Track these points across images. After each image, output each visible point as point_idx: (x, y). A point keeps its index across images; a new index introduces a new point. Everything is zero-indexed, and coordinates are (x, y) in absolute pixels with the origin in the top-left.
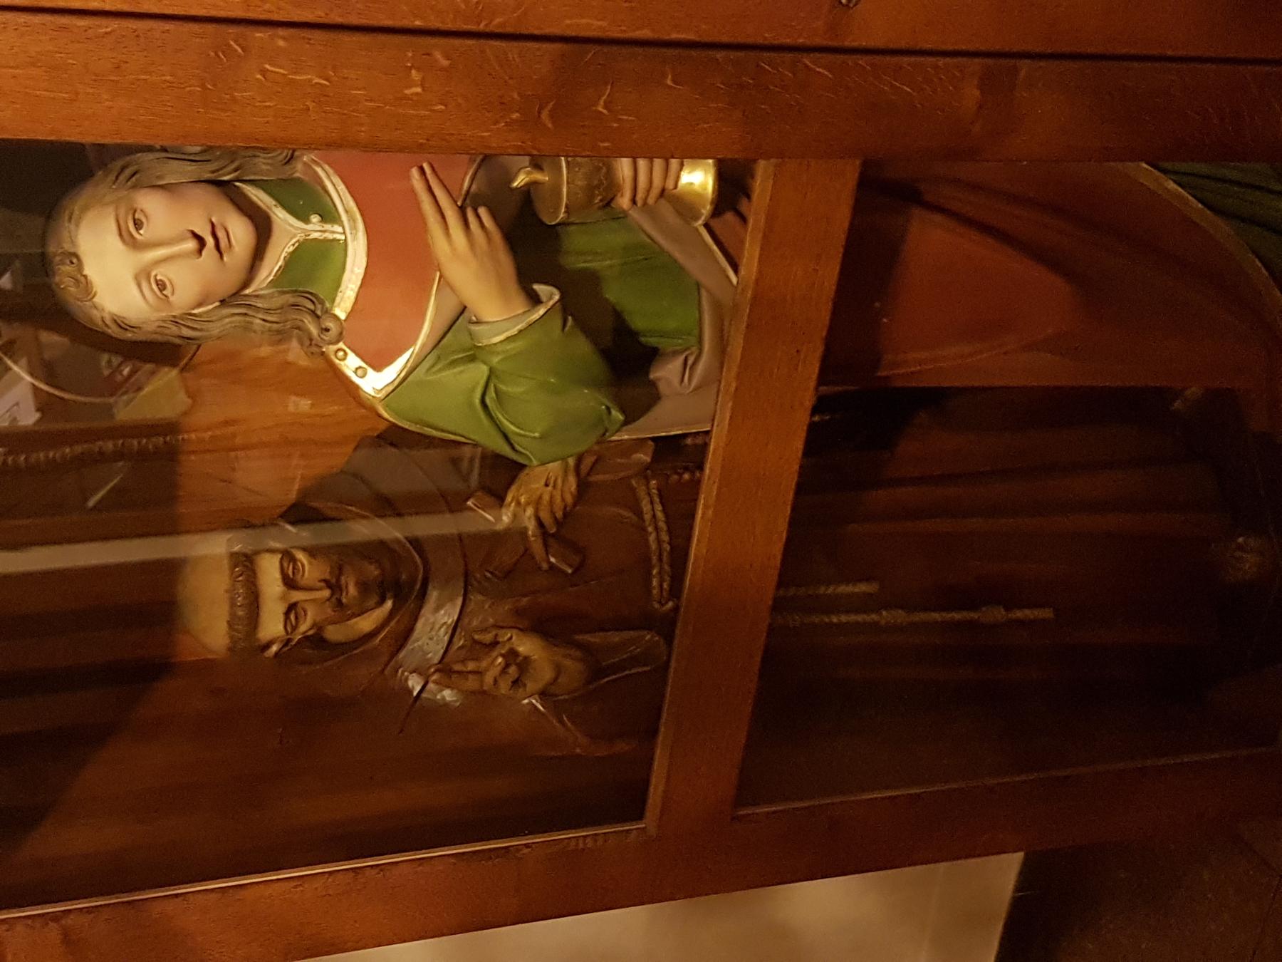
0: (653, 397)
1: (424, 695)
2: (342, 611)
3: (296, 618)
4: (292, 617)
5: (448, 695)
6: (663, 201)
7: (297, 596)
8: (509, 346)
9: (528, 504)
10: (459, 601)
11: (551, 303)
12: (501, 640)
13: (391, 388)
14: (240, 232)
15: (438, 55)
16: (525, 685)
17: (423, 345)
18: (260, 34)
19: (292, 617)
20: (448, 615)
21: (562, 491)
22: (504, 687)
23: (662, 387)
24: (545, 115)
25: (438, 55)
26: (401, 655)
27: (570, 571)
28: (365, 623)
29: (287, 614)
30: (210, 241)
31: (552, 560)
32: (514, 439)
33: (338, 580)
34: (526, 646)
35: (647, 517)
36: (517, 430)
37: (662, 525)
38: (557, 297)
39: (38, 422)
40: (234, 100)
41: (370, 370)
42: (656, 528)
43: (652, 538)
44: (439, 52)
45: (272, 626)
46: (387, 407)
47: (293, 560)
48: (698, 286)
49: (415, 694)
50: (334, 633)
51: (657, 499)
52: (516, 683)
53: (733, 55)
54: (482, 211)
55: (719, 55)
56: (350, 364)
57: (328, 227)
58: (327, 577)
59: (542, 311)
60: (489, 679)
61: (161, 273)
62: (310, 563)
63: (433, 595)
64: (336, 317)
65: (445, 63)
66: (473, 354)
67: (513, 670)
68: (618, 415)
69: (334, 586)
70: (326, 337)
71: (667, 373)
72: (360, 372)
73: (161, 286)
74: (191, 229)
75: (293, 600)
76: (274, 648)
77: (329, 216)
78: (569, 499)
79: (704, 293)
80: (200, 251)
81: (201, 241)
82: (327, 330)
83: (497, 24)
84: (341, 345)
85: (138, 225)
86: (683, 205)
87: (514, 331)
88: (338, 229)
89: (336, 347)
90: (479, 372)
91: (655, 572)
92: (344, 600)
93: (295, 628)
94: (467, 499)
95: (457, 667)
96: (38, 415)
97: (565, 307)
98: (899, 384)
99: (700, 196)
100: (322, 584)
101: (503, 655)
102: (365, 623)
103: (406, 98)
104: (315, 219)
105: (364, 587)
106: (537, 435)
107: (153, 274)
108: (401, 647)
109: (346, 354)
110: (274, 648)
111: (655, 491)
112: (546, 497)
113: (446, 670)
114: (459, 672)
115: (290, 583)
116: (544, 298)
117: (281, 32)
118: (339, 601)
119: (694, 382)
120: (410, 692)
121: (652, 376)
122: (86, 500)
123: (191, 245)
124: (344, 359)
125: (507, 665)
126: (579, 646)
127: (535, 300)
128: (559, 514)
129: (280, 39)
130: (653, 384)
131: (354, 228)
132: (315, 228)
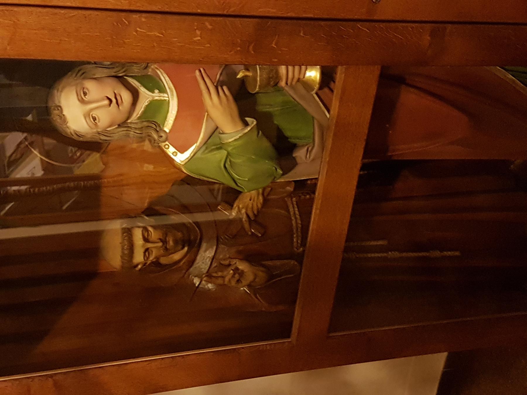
0: (294, 164)
1: (201, 286)
2: (167, 251)
3: (149, 254)
4: (147, 254)
5: (210, 286)
6: (299, 84)
7: (149, 245)
8: (235, 143)
9: (243, 208)
10: (215, 248)
11: (253, 125)
12: (232, 263)
13: (187, 160)
14: (126, 96)
15: (207, 24)
16: (242, 282)
17: (200, 143)
18: (135, 16)
19: (147, 254)
20: (210, 253)
21: (257, 203)
22: (233, 283)
23: (298, 160)
24: (251, 48)
25: (207, 24)
26: (191, 269)
27: (260, 235)
28: (177, 256)
29: (145, 253)
30: (114, 100)
31: (253, 231)
32: (237, 181)
33: (166, 239)
34: (242, 266)
35: (292, 213)
36: (238, 177)
37: (298, 216)
38: (255, 123)
39: (44, 174)
40: (124, 43)
41: (178, 153)
42: (296, 218)
43: (294, 222)
44: (208, 23)
45: (139, 257)
46: (186, 168)
47: (148, 231)
48: (313, 118)
49: (197, 285)
50: (164, 261)
51: (296, 206)
52: (238, 281)
53: (329, 23)
54: (225, 88)
55: (322, 23)
56: (170, 151)
57: (162, 95)
58: (161, 238)
59: (249, 129)
60: (227, 279)
61: (95, 114)
62: (154, 232)
63: (204, 245)
64: (165, 131)
65: (210, 27)
66: (220, 147)
67: (237, 276)
68: (280, 172)
69: (164, 241)
70: (161, 139)
71: (300, 154)
72: (174, 154)
73: (94, 119)
74: (106, 95)
75: (146, 247)
76: (140, 267)
77: (162, 90)
78: (260, 206)
79: (315, 121)
80: (110, 105)
81: (110, 101)
82: (161, 137)
83: (231, 11)
84: (167, 143)
85: (85, 94)
86: (307, 85)
87: (237, 137)
88: (166, 95)
89: (164, 144)
90: (224, 153)
91: (295, 236)
92: (168, 247)
93: (148, 258)
94: (218, 206)
95: (214, 275)
96: (42, 172)
97: (259, 127)
98: (396, 158)
99: (313, 81)
100: (159, 241)
101: (232, 270)
102: (177, 256)
103: (195, 42)
104: (157, 91)
105: (176, 242)
106: (247, 179)
107: (91, 114)
108: (191, 267)
109: (169, 146)
110: (140, 267)
111: (295, 203)
112: (250, 206)
113: (209, 276)
114: (214, 277)
115: (146, 240)
116: (250, 123)
117: (144, 15)
118: (166, 247)
119: (311, 158)
120: (195, 285)
121: (294, 155)
122: (62, 207)
123: (107, 102)
124: (168, 149)
125: (234, 274)
126: (263, 266)
127: (246, 124)
128: (256, 212)
129: (143, 18)
130: (294, 158)
131: (172, 95)
132: (157, 95)
